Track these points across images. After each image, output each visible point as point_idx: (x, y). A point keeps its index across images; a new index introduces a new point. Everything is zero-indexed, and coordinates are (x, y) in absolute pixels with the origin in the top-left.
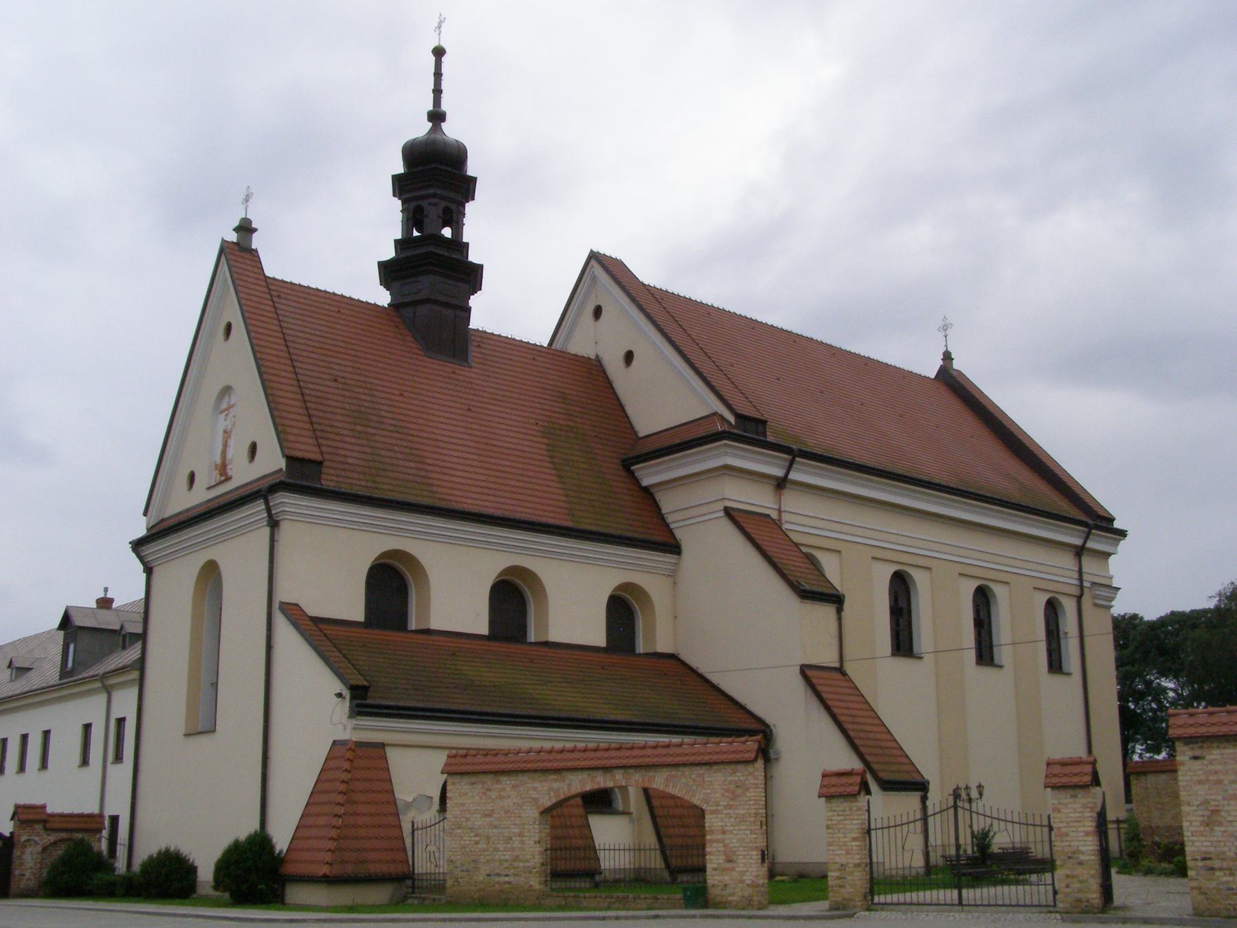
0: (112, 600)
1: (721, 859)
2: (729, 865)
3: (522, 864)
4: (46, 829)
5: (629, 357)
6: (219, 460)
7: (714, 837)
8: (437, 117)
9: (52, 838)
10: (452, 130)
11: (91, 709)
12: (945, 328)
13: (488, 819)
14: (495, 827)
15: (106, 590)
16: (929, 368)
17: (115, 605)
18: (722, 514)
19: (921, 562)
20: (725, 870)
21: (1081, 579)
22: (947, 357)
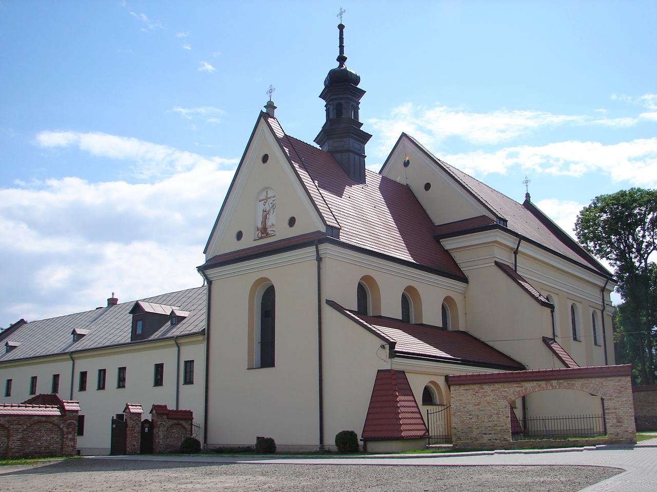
0: (117, 300)
1: (615, 421)
2: (619, 424)
3: (499, 428)
4: (168, 418)
5: (428, 186)
6: (260, 226)
7: (610, 411)
8: (342, 59)
9: (171, 423)
10: (350, 66)
11: (168, 357)
12: (527, 182)
13: (477, 407)
14: (482, 411)
15: (113, 294)
17: (118, 303)
18: (494, 264)
20: (617, 426)
21: (603, 302)
22: (528, 195)
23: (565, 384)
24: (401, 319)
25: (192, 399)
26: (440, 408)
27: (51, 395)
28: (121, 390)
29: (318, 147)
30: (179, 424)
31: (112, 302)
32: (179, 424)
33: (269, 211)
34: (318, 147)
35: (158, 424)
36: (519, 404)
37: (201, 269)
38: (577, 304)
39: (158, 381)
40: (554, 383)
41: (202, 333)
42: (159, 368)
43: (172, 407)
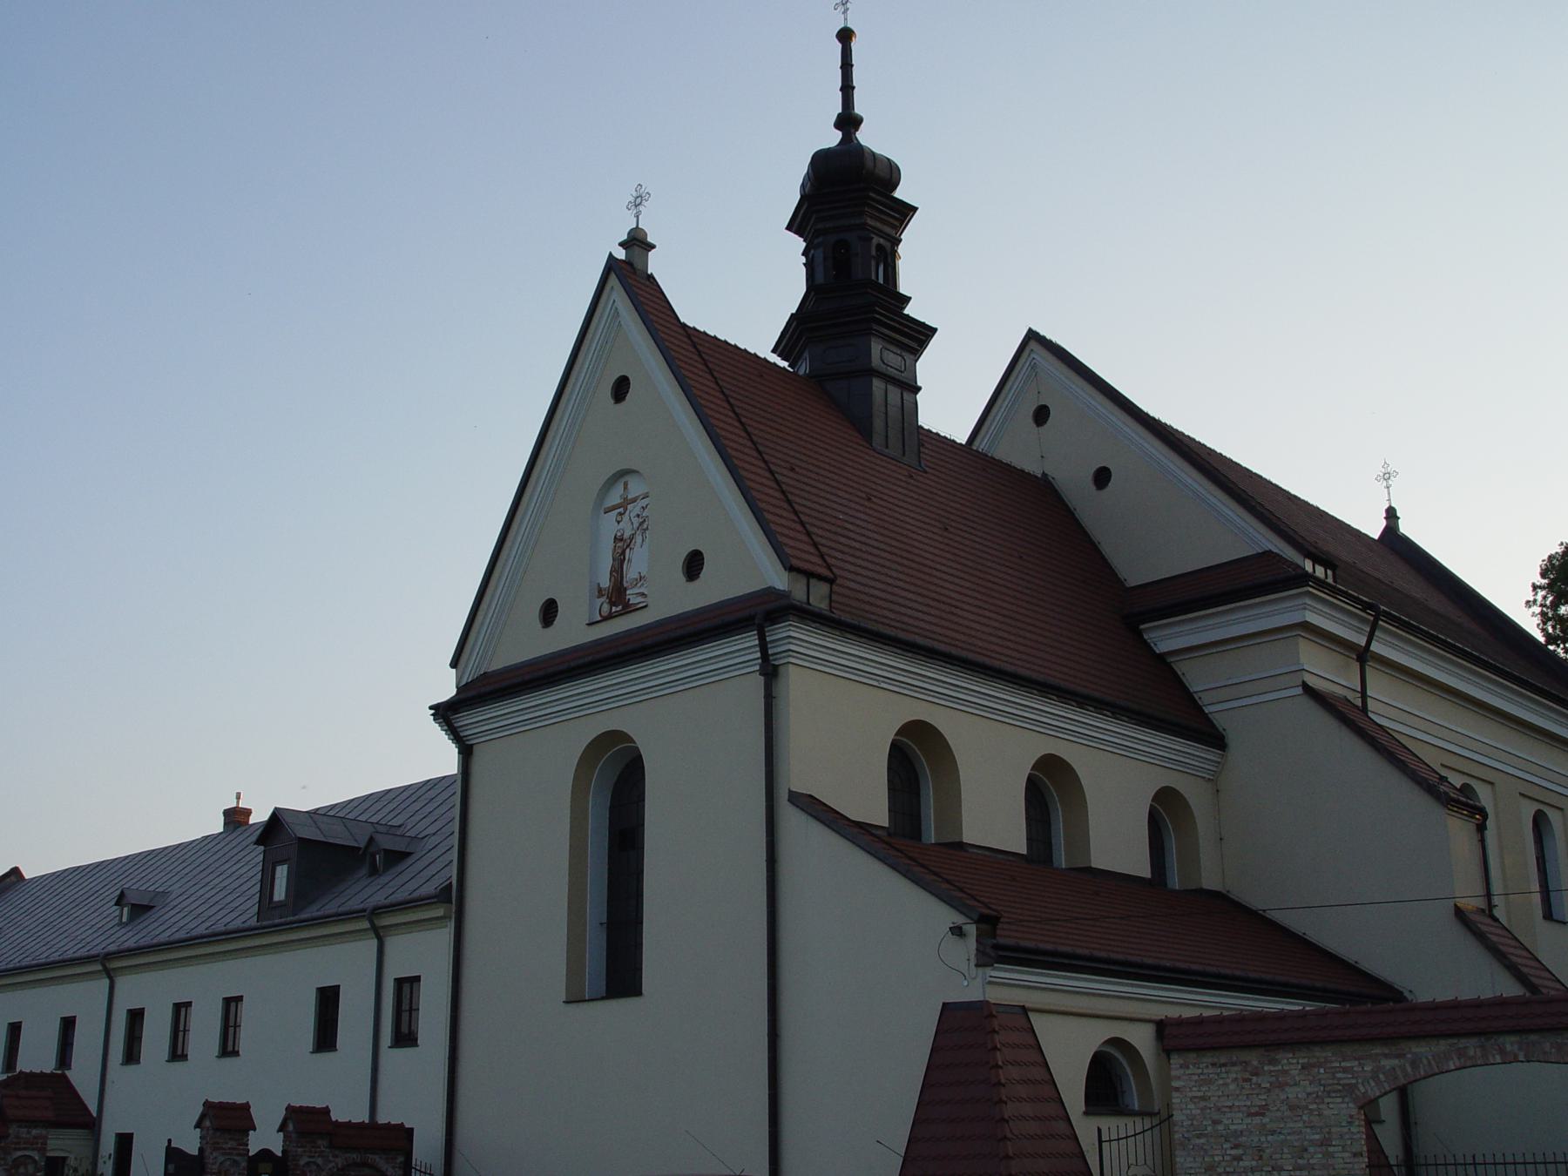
0: (248, 812)
5: (1102, 477)
6: (605, 582)
8: (848, 121)
9: (340, 1162)
11: (347, 964)
12: (1387, 477)
13: (1257, 1120)
14: (1273, 1132)
15: (238, 797)
16: (1373, 527)
18: (1300, 690)
19: (1489, 775)
22: (1391, 514)
23: (1547, 1046)
24: (1024, 851)
25: (411, 1095)
26: (1148, 1123)
27: (52, 1075)
28: (178, 1065)
29: (784, 364)
30: (365, 1164)
31: (236, 817)
32: (365, 1164)
33: (632, 537)
34: (784, 364)
35: (302, 1162)
36: (1388, 1107)
37: (444, 713)
38: (1552, 815)
39: (326, 1038)
40: (1510, 1043)
41: (444, 896)
42: (328, 1000)
43: (349, 1109)
